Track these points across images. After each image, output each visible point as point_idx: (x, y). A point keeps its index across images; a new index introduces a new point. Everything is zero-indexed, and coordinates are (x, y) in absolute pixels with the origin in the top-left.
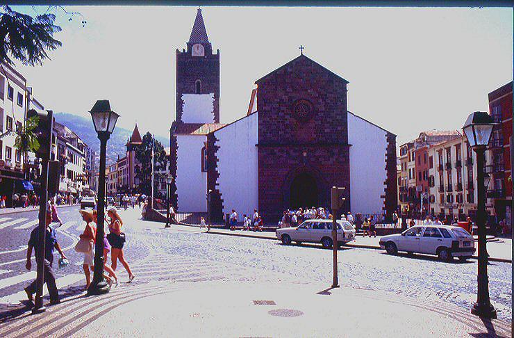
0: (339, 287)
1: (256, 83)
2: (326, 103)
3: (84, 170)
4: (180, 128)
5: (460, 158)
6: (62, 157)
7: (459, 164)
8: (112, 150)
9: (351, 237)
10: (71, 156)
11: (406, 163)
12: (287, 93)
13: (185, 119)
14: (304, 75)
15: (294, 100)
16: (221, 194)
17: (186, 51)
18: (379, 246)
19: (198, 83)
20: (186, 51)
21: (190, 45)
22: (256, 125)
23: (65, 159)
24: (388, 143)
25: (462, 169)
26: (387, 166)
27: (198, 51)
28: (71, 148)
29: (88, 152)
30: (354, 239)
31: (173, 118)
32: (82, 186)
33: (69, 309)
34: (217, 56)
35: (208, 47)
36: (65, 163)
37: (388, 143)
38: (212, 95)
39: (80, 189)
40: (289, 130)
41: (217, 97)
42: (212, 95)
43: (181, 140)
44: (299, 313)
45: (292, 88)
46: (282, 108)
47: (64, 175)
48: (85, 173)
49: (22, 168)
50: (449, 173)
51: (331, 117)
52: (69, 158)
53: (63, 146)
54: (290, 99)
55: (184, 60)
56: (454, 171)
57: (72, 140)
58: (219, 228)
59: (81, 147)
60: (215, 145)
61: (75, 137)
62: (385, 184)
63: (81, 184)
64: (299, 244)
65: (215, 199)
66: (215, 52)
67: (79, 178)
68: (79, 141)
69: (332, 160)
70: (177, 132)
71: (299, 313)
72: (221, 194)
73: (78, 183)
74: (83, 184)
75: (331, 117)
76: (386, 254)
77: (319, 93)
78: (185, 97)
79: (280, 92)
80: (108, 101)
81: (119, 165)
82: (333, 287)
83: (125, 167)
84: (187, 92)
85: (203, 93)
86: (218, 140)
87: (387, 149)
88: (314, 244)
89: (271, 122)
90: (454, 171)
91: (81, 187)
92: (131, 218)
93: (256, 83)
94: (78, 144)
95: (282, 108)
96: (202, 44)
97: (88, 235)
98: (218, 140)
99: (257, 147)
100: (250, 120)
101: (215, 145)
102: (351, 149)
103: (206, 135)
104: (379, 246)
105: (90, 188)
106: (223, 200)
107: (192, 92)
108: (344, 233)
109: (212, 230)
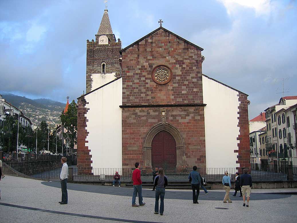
2: (182, 68)
11: (270, 124)
14: (163, 44)
15: (154, 66)
16: (90, 151)
19: (104, 65)
20: (95, 41)
21: (98, 36)
24: (240, 102)
27: (104, 41)
37: (240, 102)
40: (149, 93)
45: (152, 56)
46: (144, 74)
49: (164, 174)
54: (151, 66)
58: (175, 189)
60: (85, 107)
69: (188, 118)
72: (90, 151)
79: (142, 61)
84: (95, 72)
86: (88, 103)
88: (187, 187)
89: (134, 86)
92: (119, 181)
95: (144, 74)
97: (141, 204)
98: (88, 103)
101: (85, 107)
102: (206, 109)
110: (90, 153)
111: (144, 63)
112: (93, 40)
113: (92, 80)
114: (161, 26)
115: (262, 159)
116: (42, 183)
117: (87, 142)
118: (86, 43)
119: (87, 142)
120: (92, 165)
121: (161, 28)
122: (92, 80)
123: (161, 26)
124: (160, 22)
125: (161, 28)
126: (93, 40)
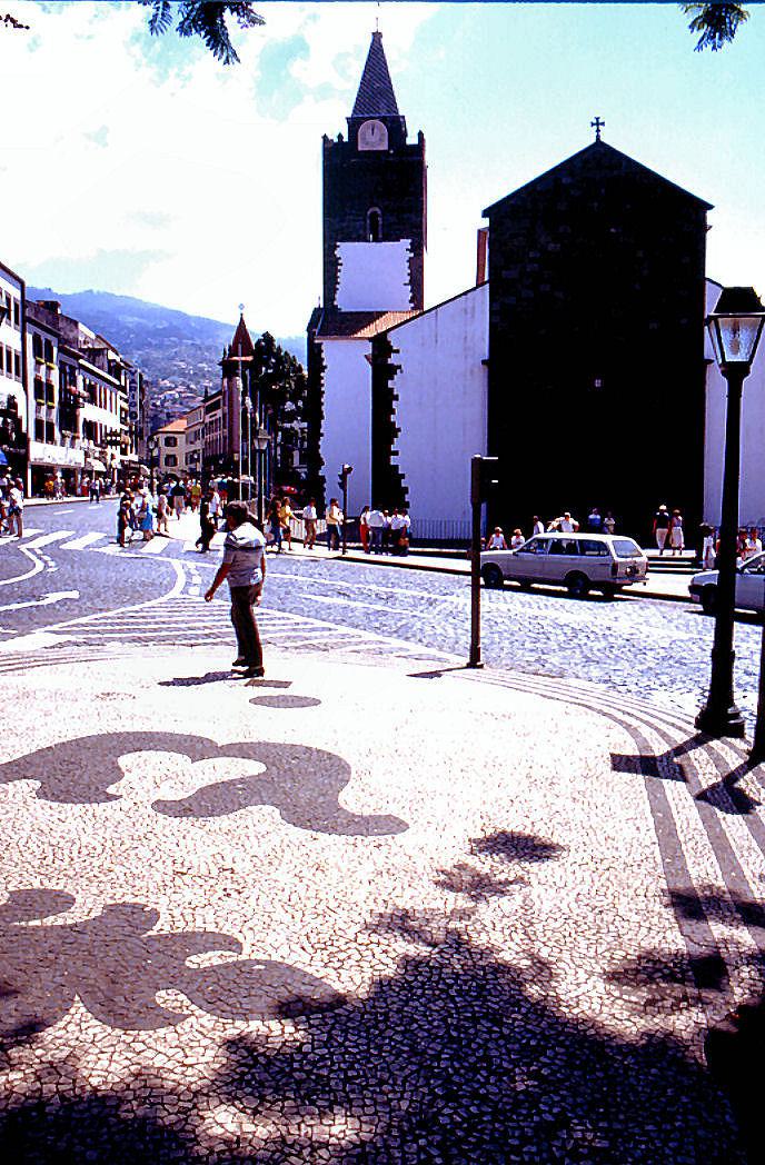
0: (481, 667)
1: (486, 213)
3: (123, 421)
4: (330, 321)
6: (70, 391)
8: (204, 376)
9: (634, 574)
10: (90, 389)
13: (343, 302)
16: (403, 476)
17: (346, 139)
18: (689, 595)
20: (346, 139)
21: (354, 124)
22: (483, 312)
23: (77, 396)
27: (374, 139)
28: (92, 372)
29: (133, 381)
30: (643, 578)
31: (315, 298)
32: (118, 457)
34: (419, 149)
35: (396, 126)
36: (77, 405)
37: (322, 374)
38: (406, 243)
39: (116, 464)
41: (418, 248)
42: (406, 243)
43: (332, 349)
44: (316, 702)
47: (76, 430)
48: (127, 428)
52: (86, 394)
53: (71, 367)
55: (340, 160)
57: (94, 354)
59: (115, 369)
61: (103, 346)
63: (116, 451)
64: (526, 587)
65: (389, 491)
66: (412, 140)
67: (111, 439)
68: (111, 355)
70: (324, 333)
71: (316, 702)
72: (403, 476)
73: (110, 450)
74: (123, 452)
76: (700, 613)
78: (344, 250)
80: (479, 231)
81: (208, 410)
82: (469, 666)
83: (219, 413)
85: (387, 238)
86: (397, 351)
91: (116, 457)
93: (484, 216)
94: (110, 361)
96: (383, 120)
98: (397, 351)
99: (486, 367)
100: (470, 305)
101: (389, 361)
103: (370, 339)
104: (689, 595)
105: (141, 462)
106: (406, 490)
108: (615, 566)
109: (351, 554)
110: (407, 498)
111: (548, 243)
112: (340, 136)
113: (340, 262)
114: (598, 137)
115: (489, 448)
116: (63, 901)
117: (396, 453)
118: (321, 141)
119: (396, 453)
120: (323, 355)
121: (599, 143)
122: (340, 262)
123: (598, 137)
124: (598, 124)
125: (599, 143)
126: (340, 136)
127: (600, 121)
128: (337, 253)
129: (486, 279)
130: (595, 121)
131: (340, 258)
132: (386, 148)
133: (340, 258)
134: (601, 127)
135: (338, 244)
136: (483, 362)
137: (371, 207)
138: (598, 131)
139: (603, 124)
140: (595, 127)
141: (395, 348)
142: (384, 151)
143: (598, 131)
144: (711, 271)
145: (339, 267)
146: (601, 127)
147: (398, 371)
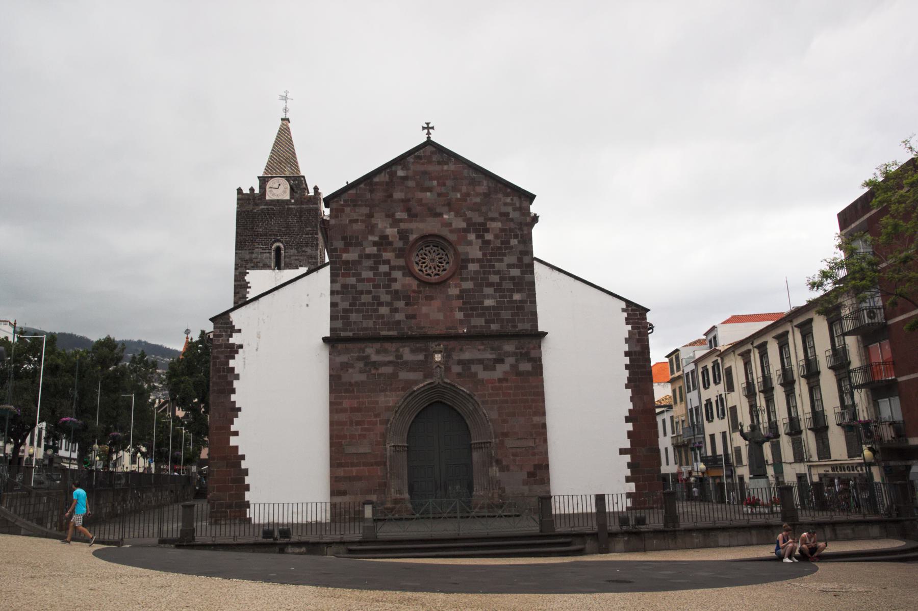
5: (790, 363)
7: (788, 384)
12: (395, 223)
15: (413, 237)
16: (243, 457)
17: (257, 191)
19: (278, 250)
20: (257, 191)
21: (263, 181)
24: (629, 327)
25: (797, 386)
26: (629, 379)
27: (279, 191)
33: (557, 505)
37: (629, 327)
40: (401, 304)
50: (770, 400)
51: (498, 273)
56: (779, 394)
60: (231, 341)
62: (627, 421)
69: (501, 370)
72: (243, 457)
75: (498, 273)
77: (469, 221)
84: (256, 267)
86: (239, 331)
87: (627, 341)
90: (779, 394)
98: (239, 331)
101: (231, 341)
107: (266, 266)
112: (252, 189)
113: (249, 285)
114: (429, 138)
117: (236, 434)
119: (236, 434)
121: (429, 142)
122: (249, 285)
123: (429, 138)
124: (428, 128)
125: (429, 142)
126: (252, 189)
127: (430, 126)
128: (247, 278)
129: (327, 260)
130: (426, 126)
131: (249, 283)
132: (288, 197)
133: (249, 283)
134: (431, 131)
135: (247, 271)
136: (325, 340)
137: (275, 242)
138: (429, 133)
139: (433, 128)
140: (426, 131)
141: (236, 328)
142: (287, 200)
143: (429, 133)
144: (531, 211)
145: (248, 290)
146: (431, 131)
147: (240, 350)
